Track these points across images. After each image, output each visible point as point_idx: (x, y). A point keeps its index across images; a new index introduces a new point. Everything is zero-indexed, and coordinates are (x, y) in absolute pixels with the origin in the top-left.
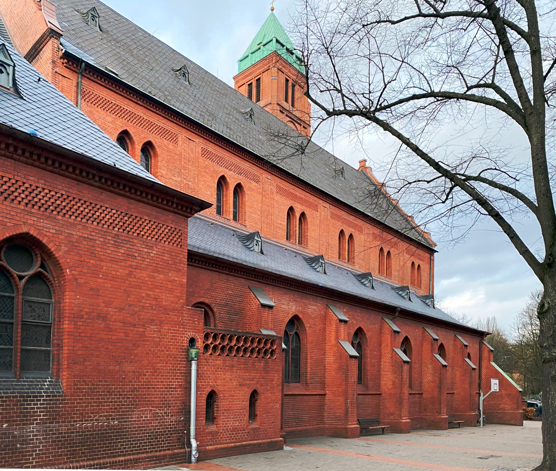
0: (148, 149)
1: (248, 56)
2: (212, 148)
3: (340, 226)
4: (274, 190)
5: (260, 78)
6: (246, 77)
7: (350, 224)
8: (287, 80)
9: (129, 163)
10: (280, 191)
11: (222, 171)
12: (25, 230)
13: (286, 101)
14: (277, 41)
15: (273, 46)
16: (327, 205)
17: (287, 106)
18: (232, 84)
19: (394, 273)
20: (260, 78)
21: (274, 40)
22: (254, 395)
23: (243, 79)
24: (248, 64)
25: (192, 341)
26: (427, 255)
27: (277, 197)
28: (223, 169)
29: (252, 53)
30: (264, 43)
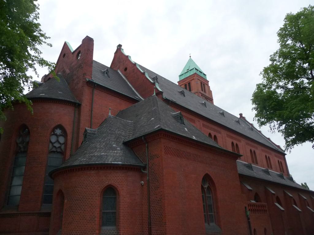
0: (215, 138)
1: (183, 74)
2: (205, 123)
3: (250, 148)
4: (226, 135)
5: (190, 83)
6: (183, 82)
7: (215, 130)
8: (201, 83)
9: (211, 142)
10: (228, 136)
11: (209, 131)
12: (59, 124)
13: (202, 91)
14: (196, 69)
15: (195, 71)
16: (244, 139)
17: (203, 92)
18: (177, 84)
19: (273, 166)
20: (190, 83)
21: (194, 69)
22: (265, 229)
23: (182, 82)
24: (183, 77)
25: (246, 207)
26: (282, 157)
27: (227, 139)
28: (209, 130)
29: (185, 73)
30: (190, 69)
